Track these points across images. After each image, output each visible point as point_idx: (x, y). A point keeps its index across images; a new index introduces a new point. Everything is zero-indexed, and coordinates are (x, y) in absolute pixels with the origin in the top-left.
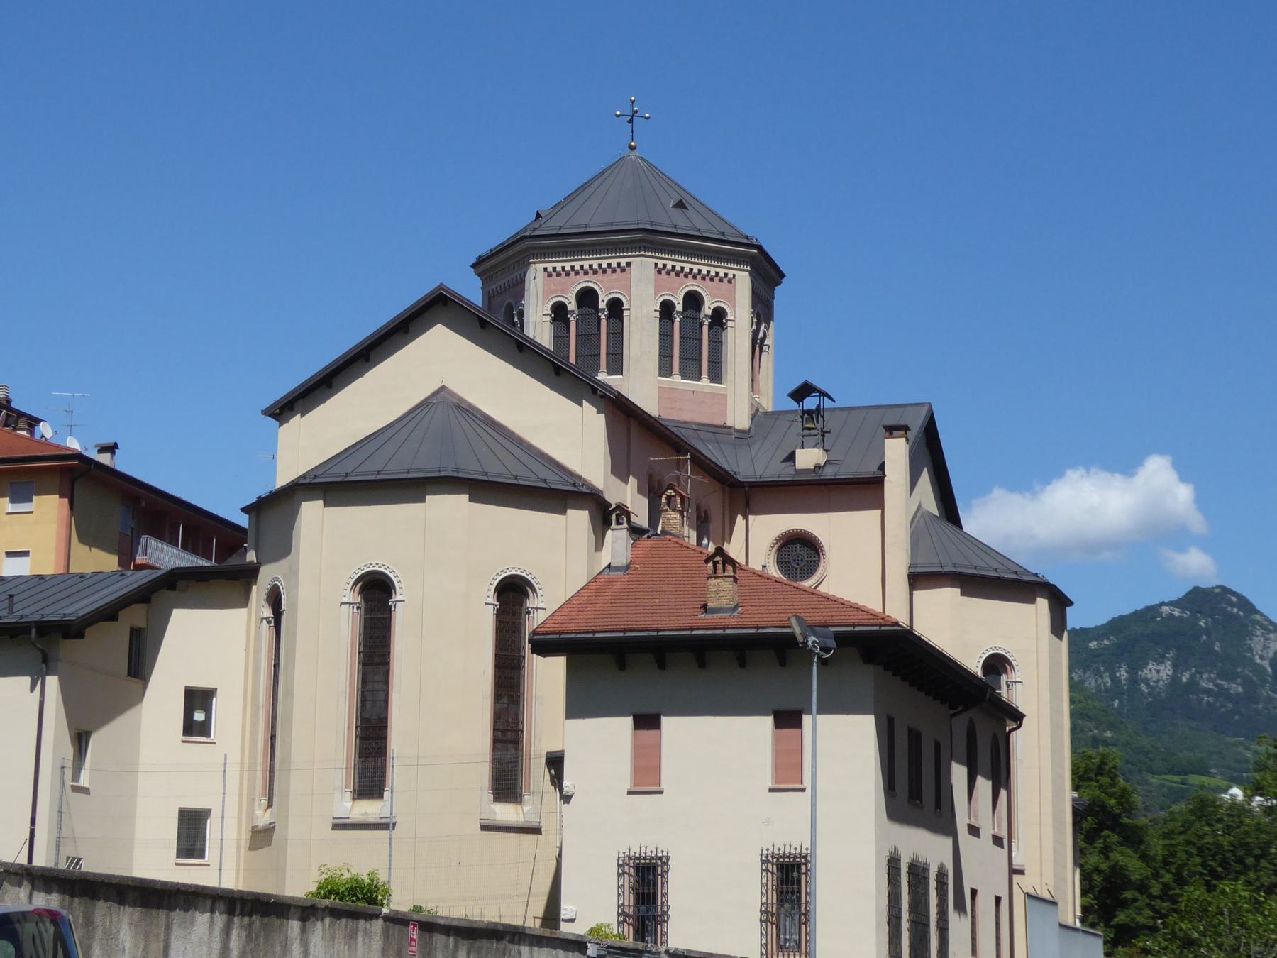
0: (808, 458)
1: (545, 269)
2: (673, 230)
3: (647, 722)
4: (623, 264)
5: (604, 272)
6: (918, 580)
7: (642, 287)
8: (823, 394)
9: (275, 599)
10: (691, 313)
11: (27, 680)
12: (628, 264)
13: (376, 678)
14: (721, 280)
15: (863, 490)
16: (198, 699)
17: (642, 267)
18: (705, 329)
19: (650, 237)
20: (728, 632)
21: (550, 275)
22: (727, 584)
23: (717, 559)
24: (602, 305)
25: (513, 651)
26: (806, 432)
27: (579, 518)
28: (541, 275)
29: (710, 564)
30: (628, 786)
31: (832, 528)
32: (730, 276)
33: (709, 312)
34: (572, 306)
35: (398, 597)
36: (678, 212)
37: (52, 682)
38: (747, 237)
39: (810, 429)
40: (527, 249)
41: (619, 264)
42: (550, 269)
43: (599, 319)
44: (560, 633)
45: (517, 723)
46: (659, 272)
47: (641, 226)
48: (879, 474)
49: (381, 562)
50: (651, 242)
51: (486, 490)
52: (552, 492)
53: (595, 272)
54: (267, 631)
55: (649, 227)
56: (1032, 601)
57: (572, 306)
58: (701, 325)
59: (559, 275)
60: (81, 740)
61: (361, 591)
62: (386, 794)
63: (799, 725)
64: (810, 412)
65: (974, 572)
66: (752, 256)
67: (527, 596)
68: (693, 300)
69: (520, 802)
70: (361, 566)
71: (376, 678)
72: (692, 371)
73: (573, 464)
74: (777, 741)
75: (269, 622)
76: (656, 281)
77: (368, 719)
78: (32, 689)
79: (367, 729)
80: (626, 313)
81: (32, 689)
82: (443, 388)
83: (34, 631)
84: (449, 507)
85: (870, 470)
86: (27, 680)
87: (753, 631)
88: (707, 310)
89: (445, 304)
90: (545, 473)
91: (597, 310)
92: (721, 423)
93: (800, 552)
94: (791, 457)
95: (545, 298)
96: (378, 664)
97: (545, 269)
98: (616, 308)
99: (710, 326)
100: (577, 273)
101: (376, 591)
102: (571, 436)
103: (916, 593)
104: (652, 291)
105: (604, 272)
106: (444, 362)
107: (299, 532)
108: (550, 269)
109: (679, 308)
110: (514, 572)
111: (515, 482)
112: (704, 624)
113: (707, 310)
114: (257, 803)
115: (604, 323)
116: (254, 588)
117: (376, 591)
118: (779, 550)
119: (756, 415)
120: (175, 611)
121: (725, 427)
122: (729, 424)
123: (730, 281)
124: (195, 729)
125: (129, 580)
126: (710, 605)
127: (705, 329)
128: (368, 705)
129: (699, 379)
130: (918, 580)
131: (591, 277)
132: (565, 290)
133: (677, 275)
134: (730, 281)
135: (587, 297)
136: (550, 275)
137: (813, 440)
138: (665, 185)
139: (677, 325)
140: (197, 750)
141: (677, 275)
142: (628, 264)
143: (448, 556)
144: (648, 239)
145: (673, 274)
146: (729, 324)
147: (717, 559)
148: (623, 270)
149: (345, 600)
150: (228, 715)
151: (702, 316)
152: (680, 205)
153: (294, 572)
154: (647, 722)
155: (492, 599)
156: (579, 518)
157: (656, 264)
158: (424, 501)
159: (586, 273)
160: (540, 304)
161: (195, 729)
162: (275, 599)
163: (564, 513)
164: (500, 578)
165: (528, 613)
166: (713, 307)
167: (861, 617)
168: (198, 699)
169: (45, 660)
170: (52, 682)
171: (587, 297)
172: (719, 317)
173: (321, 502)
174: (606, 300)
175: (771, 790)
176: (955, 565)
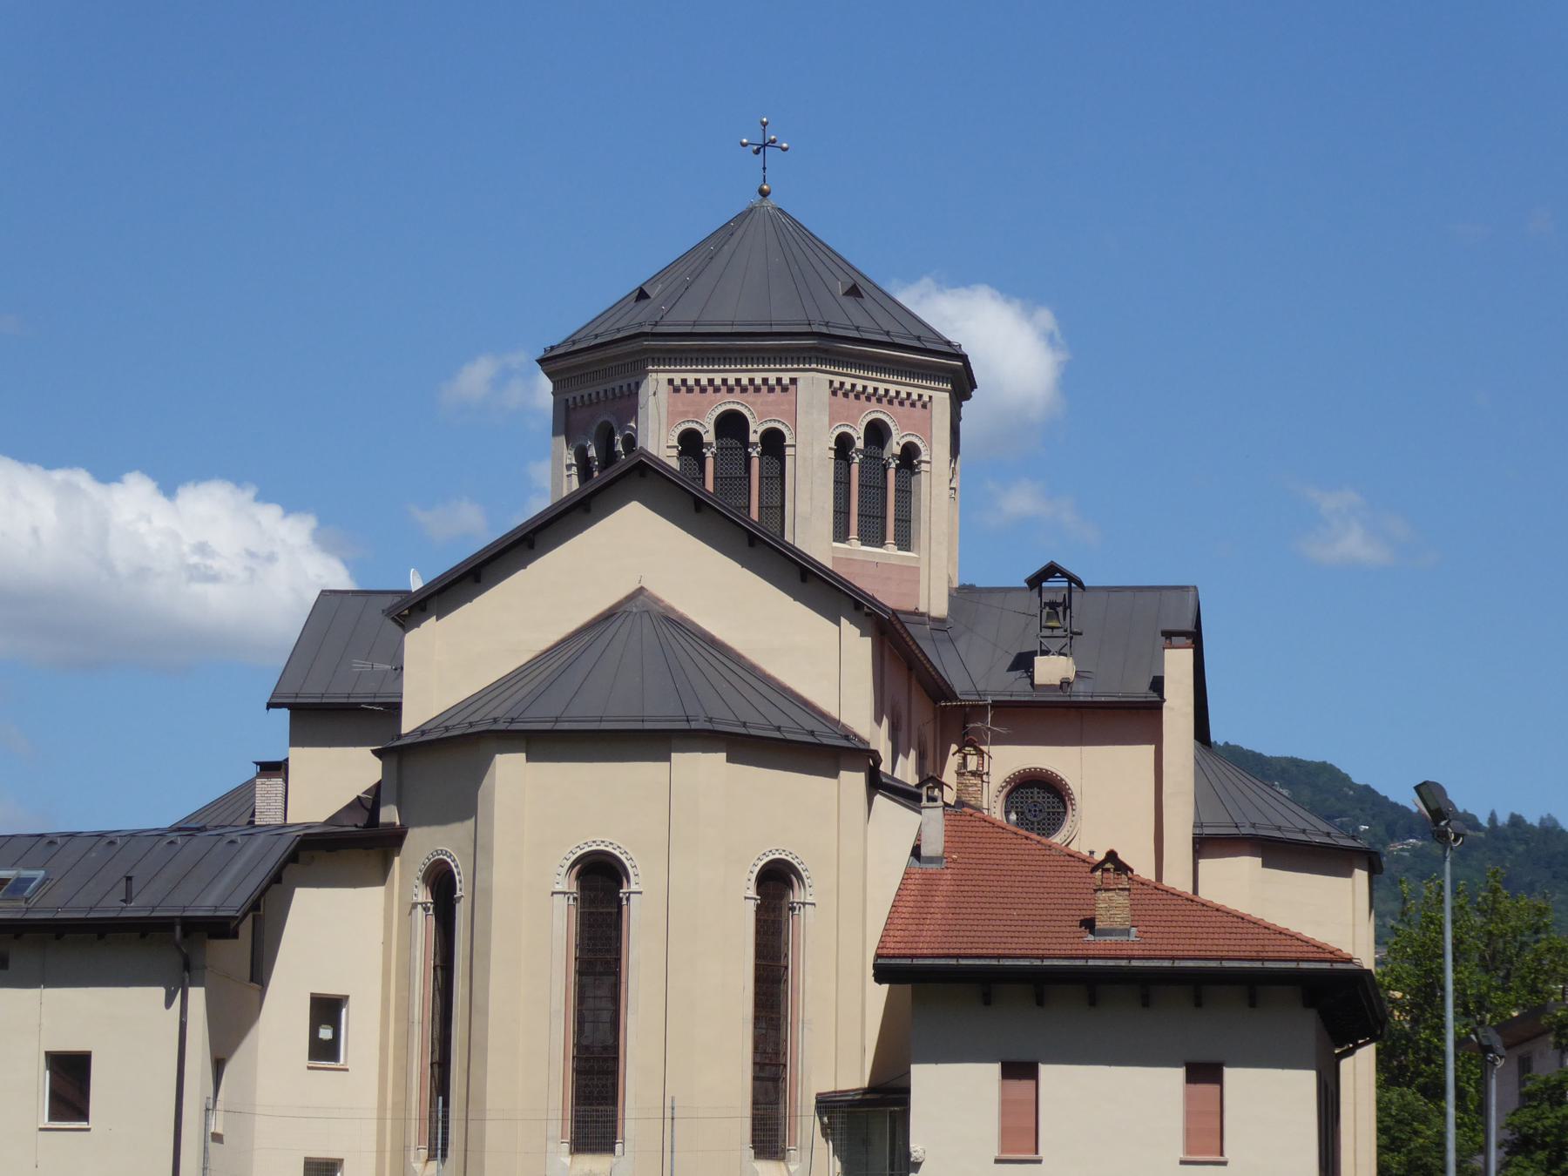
0: (1051, 669)
1: (671, 381)
2: (855, 334)
3: (1020, 1070)
4: (786, 381)
5: (757, 390)
6: (1206, 845)
7: (812, 415)
8: (1071, 579)
9: (441, 881)
10: (873, 450)
11: (160, 992)
12: (793, 381)
13: (599, 993)
14: (913, 405)
15: (1135, 718)
16: (327, 1009)
17: (813, 384)
18: (891, 473)
19: (827, 344)
20: (1135, 963)
21: (677, 390)
22: (1121, 899)
23: (1108, 865)
24: (754, 438)
25: (591, 914)
26: (1047, 632)
27: (854, 781)
28: (664, 389)
29: (1099, 873)
30: (996, 1154)
31: (1087, 769)
32: (926, 398)
33: (897, 450)
34: (709, 437)
35: (634, 888)
36: (849, 304)
37: (197, 995)
38: (949, 343)
39: (1053, 628)
40: (645, 350)
41: (779, 380)
42: (677, 382)
43: (748, 458)
44: (912, 957)
45: (777, 1054)
46: (834, 393)
47: (815, 329)
48: (1154, 697)
49: (599, 839)
50: (826, 351)
51: (748, 747)
52: (817, 749)
53: (744, 390)
54: (423, 925)
55: (824, 330)
56: (1348, 873)
57: (709, 437)
58: (885, 469)
59: (690, 390)
60: (219, 1065)
61: (578, 877)
62: (618, 1147)
63: (1218, 1079)
64: (1053, 605)
65: (1277, 834)
66: (953, 370)
67: (791, 886)
68: (877, 433)
69: (783, 1159)
70: (581, 843)
71: (599, 993)
72: (872, 535)
73: (828, 705)
74: (1189, 1099)
75: (426, 909)
76: (831, 405)
77: (587, 1048)
78: (168, 1004)
79: (587, 1060)
80: (789, 451)
81: (168, 1004)
82: (642, 589)
83: (178, 928)
84: (703, 769)
85: (1139, 690)
86: (160, 992)
87: (1167, 964)
88: (895, 446)
89: (643, 475)
90: (810, 723)
91: (746, 443)
92: (912, 608)
93: (1042, 798)
94: (1024, 663)
95: (671, 424)
96: (601, 974)
97: (671, 381)
98: (774, 442)
99: (898, 468)
100: (717, 390)
101: (600, 879)
102: (830, 670)
103: (1203, 863)
104: (826, 419)
105: (757, 390)
106: (639, 553)
107: (491, 794)
108: (677, 382)
109: (860, 444)
110: (777, 856)
111: (777, 735)
112: (1096, 950)
113: (895, 446)
114: (412, 1154)
115: (755, 463)
116: (397, 860)
117: (600, 879)
118: (1008, 796)
119: (963, 595)
120: (298, 890)
121: (916, 613)
122: (922, 609)
123: (924, 406)
124: (324, 1052)
125: (249, 852)
126: (1099, 925)
127: (891, 473)
128: (588, 1027)
129: (882, 544)
130: (1206, 845)
131: (737, 395)
132: (700, 414)
133: (846, 395)
134: (924, 406)
135: (731, 425)
136: (677, 390)
137: (1055, 645)
138: (820, 254)
139: (855, 469)
140: (324, 1080)
141: (857, 397)
142: (793, 381)
143: (693, 827)
144: (824, 348)
145: (852, 395)
146: (924, 467)
147: (1108, 865)
148: (785, 389)
149: (559, 888)
150: (361, 1030)
151: (886, 454)
152: (854, 292)
153: (478, 848)
154: (1020, 1070)
155: (752, 893)
156: (854, 781)
157: (831, 382)
158: (668, 759)
159: (730, 390)
160: (663, 432)
161: (324, 1052)
162: (441, 881)
163: (835, 775)
164: (761, 864)
165: (793, 909)
166: (902, 442)
167: (1294, 950)
168: (327, 1009)
169: (187, 967)
170: (197, 995)
171: (731, 425)
172: (909, 455)
173: (523, 756)
174: (760, 430)
175: (1183, 1162)
176: (1253, 825)
